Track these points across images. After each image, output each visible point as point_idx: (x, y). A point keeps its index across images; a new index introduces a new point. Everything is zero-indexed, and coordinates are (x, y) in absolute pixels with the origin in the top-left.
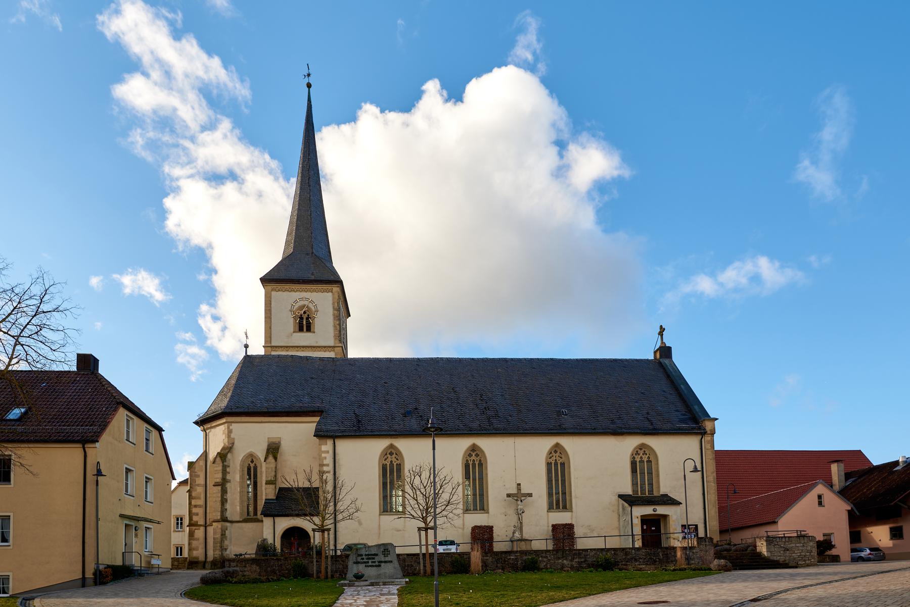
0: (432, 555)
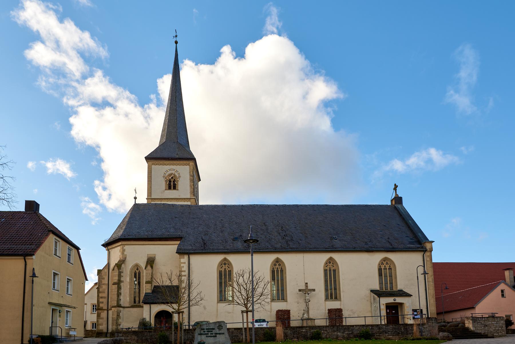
0: (250, 329)
